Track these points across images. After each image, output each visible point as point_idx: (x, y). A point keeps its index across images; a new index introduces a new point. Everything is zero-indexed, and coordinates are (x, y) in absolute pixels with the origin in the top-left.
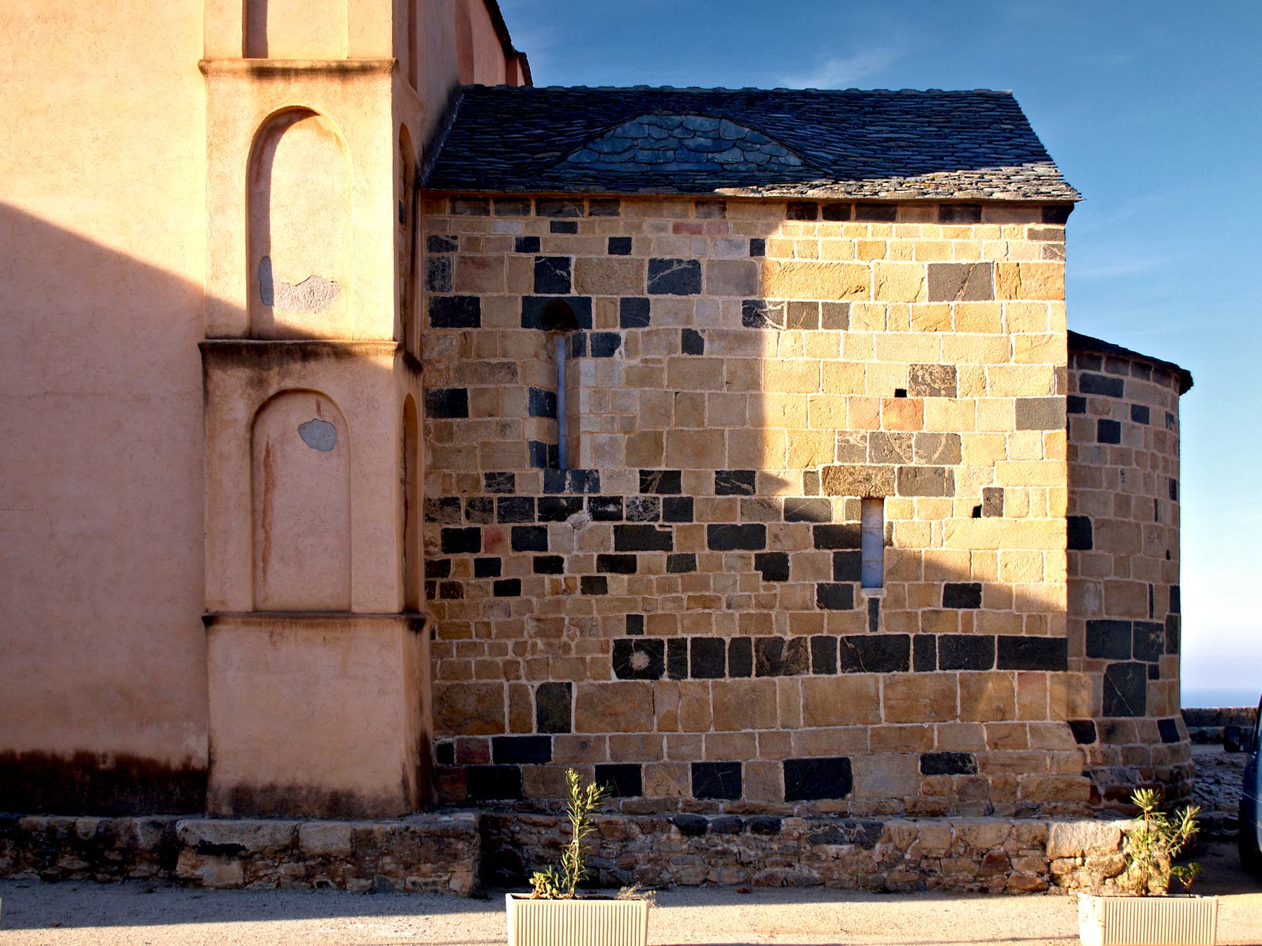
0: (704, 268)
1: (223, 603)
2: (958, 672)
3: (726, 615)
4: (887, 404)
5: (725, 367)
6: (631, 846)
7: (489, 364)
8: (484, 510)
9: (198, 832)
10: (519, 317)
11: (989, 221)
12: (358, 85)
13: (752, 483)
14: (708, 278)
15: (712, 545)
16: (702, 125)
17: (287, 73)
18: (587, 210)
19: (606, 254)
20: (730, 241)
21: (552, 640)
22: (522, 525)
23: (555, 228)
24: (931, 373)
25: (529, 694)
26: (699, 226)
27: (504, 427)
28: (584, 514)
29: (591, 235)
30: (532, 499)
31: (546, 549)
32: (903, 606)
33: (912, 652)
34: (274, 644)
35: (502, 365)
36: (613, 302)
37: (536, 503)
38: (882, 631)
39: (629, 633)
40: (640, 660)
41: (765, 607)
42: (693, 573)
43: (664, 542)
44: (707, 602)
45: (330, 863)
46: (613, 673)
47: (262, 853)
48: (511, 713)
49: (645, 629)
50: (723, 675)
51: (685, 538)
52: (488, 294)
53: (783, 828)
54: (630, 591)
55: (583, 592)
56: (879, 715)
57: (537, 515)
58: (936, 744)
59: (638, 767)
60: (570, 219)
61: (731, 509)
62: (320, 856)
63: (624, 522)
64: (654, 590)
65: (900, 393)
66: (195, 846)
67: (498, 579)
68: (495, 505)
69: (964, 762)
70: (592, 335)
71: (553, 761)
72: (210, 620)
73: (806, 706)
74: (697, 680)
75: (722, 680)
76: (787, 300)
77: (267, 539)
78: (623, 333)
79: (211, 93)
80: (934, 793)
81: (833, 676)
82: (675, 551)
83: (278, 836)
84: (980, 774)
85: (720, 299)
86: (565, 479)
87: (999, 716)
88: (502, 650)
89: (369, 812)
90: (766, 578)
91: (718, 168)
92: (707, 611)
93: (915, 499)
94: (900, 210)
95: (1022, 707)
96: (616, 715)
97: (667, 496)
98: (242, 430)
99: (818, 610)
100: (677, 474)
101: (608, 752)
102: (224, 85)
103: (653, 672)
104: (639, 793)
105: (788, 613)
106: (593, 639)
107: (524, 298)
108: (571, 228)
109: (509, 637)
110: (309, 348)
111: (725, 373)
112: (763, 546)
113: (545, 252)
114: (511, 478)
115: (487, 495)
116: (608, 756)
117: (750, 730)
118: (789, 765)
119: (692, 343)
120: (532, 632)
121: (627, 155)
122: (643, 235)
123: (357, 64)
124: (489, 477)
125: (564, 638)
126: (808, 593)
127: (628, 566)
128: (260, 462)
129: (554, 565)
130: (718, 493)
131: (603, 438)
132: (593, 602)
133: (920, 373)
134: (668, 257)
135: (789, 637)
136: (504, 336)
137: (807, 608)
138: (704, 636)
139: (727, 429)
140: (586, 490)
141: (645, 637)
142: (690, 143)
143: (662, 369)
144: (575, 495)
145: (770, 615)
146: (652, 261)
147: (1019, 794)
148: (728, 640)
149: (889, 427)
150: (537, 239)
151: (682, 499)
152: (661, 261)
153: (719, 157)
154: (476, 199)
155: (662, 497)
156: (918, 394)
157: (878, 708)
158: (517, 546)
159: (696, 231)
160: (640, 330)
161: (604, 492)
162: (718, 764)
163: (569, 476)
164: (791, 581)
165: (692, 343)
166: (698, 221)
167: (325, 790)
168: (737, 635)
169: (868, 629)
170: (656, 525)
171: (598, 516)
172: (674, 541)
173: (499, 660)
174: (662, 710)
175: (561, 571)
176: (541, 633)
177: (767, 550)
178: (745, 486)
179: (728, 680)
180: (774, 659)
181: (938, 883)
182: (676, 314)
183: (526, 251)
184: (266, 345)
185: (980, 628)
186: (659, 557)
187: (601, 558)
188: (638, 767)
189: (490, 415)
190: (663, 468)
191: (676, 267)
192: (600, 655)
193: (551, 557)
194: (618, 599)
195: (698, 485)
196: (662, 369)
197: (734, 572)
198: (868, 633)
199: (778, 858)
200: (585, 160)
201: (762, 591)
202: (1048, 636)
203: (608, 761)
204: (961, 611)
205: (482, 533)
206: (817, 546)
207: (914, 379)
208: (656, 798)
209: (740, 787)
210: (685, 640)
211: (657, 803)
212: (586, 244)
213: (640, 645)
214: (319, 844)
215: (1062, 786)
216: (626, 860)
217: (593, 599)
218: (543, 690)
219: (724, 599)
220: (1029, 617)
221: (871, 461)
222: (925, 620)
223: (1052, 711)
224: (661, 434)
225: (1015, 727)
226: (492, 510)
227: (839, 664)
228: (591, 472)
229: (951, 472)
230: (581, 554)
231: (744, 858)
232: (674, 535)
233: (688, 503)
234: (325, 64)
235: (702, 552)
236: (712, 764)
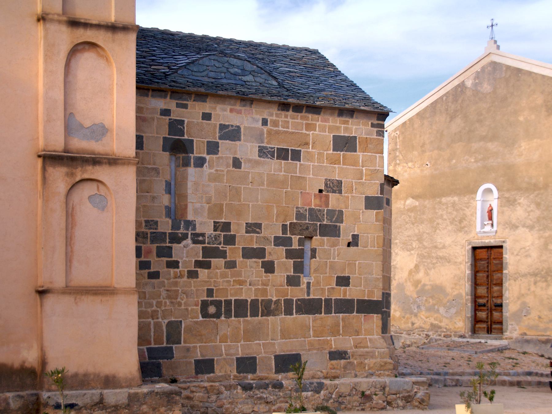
0: (242, 130)
1: (51, 282)
2: (341, 315)
3: (248, 289)
4: (315, 195)
5: (250, 175)
6: (222, 396)
7: (147, 168)
8: (144, 237)
9: (55, 398)
10: (161, 147)
11: (357, 118)
12: (120, 36)
13: (260, 229)
14: (244, 134)
15: (244, 256)
16: (236, 63)
17: (86, 25)
18: (193, 99)
19: (200, 120)
20: (253, 118)
21: (173, 300)
22: (161, 245)
23: (178, 105)
24: (333, 183)
25: (162, 326)
26: (241, 110)
27: (154, 198)
28: (189, 241)
29: (194, 110)
30: (166, 233)
31: (172, 257)
32: (320, 286)
33: (323, 306)
34: (76, 303)
35: (153, 169)
36: (203, 142)
37: (168, 235)
38: (312, 297)
39: (207, 297)
40: (212, 310)
41: (265, 285)
42: (235, 269)
43: (222, 254)
44: (241, 283)
45: (118, 410)
46: (200, 316)
47: (85, 407)
48: (154, 335)
49: (214, 295)
50: (247, 316)
51: (232, 253)
52: (147, 135)
53: (284, 385)
54: (209, 277)
55: (188, 277)
56: (310, 334)
57: (168, 240)
58: (333, 346)
59: (213, 360)
60: (185, 102)
61: (252, 240)
62: (113, 406)
63: (206, 245)
64: (219, 277)
65: (321, 191)
66: (53, 405)
67: (150, 271)
68: (149, 235)
69: (345, 354)
70: (194, 157)
71: (175, 358)
72: (42, 293)
73: (281, 330)
74: (236, 319)
75: (247, 318)
76: (276, 147)
77: (72, 251)
78: (208, 157)
79: (46, 30)
80: (334, 369)
81: (292, 317)
82: (228, 259)
83: (94, 398)
84: (351, 360)
85: (249, 144)
86: (181, 224)
87: (356, 334)
88: (151, 305)
89: (124, 384)
90: (266, 272)
91: (244, 83)
92: (241, 287)
93: (325, 238)
94: (323, 110)
95: (365, 330)
96: (201, 335)
97: (225, 233)
98: (62, 198)
99: (286, 287)
100: (229, 224)
101: (199, 353)
102: (53, 27)
103: (217, 315)
104: (213, 372)
105: (274, 288)
106: (192, 299)
107: (164, 138)
108: (185, 106)
109: (154, 299)
110: (97, 159)
111: (250, 178)
112: (264, 257)
113: (173, 117)
114: (156, 223)
115: (145, 230)
116: (199, 355)
117: (258, 342)
118: (276, 357)
119: (237, 163)
120: (164, 296)
121: (204, 74)
122: (217, 112)
123: (121, 26)
124: (146, 222)
125: (179, 300)
126: (283, 279)
127: (206, 265)
128: (70, 215)
129: (174, 265)
130: (246, 233)
131: (198, 205)
132: (192, 282)
133: (328, 183)
134: (227, 124)
135: (274, 299)
136: (154, 155)
137: (282, 286)
138: (239, 298)
139: (251, 204)
140: (190, 229)
141: (214, 299)
142: (232, 70)
143: (224, 175)
144: (185, 232)
145: (267, 289)
146: (221, 125)
147: (367, 368)
148: (249, 300)
149: (315, 205)
150: (170, 110)
151: (231, 235)
152: (224, 125)
153: (244, 78)
154: (144, 89)
155: (223, 234)
156: (328, 192)
157: (310, 331)
158: (158, 256)
159: (239, 112)
160: (215, 156)
161: (198, 231)
162: (247, 358)
163: (182, 223)
164: (276, 274)
165: (237, 163)
166: (240, 108)
167: (102, 375)
168: (253, 298)
169: (306, 295)
170: (220, 246)
171: (195, 242)
172: (228, 254)
173: (149, 310)
174: (221, 333)
175: (178, 267)
176: (169, 297)
177: (266, 259)
178: (258, 230)
179: (249, 318)
180: (267, 309)
181: (345, 408)
182: (230, 149)
183: (165, 115)
184: (77, 157)
185: (350, 295)
186: (220, 262)
187: (196, 261)
188: (213, 360)
189: (148, 193)
190: (223, 220)
191: (230, 128)
192: (195, 307)
193: (174, 261)
194: (203, 281)
195: (238, 229)
196: (224, 175)
197: (252, 269)
198: (306, 297)
199: (282, 399)
200: (186, 74)
201: (264, 278)
202: (375, 299)
203: (200, 358)
204: (342, 288)
205: (143, 248)
206: (286, 258)
207: (326, 185)
208: (220, 374)
209: (256, 367)
210: (231, 300)
211: (222, 376)
212: (192, 113)
213: (213, 303)
214: (114, 401)
215: (383, 364)
216: (219, 403)
217: (192, 281)
218: (169, 324)
219: (248, 281)
220: (368, 291)
221: (309, 221)
222: (329, 291)
223: (377, 332)
224: (223, 205)
225: (363, 339)
226: (147, 238)
227: (294, 311)
228: (192, 221)
229: (340, 227)
230: (187, 260)
231: (269, 400)
232: (228, 251)
233: (234, 237)
234: (105, 23)
235: (239, 260)
236: (244, 358)
